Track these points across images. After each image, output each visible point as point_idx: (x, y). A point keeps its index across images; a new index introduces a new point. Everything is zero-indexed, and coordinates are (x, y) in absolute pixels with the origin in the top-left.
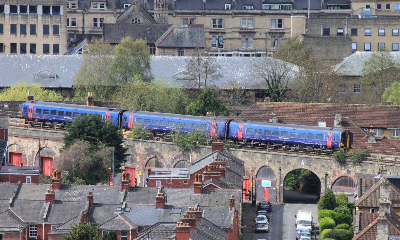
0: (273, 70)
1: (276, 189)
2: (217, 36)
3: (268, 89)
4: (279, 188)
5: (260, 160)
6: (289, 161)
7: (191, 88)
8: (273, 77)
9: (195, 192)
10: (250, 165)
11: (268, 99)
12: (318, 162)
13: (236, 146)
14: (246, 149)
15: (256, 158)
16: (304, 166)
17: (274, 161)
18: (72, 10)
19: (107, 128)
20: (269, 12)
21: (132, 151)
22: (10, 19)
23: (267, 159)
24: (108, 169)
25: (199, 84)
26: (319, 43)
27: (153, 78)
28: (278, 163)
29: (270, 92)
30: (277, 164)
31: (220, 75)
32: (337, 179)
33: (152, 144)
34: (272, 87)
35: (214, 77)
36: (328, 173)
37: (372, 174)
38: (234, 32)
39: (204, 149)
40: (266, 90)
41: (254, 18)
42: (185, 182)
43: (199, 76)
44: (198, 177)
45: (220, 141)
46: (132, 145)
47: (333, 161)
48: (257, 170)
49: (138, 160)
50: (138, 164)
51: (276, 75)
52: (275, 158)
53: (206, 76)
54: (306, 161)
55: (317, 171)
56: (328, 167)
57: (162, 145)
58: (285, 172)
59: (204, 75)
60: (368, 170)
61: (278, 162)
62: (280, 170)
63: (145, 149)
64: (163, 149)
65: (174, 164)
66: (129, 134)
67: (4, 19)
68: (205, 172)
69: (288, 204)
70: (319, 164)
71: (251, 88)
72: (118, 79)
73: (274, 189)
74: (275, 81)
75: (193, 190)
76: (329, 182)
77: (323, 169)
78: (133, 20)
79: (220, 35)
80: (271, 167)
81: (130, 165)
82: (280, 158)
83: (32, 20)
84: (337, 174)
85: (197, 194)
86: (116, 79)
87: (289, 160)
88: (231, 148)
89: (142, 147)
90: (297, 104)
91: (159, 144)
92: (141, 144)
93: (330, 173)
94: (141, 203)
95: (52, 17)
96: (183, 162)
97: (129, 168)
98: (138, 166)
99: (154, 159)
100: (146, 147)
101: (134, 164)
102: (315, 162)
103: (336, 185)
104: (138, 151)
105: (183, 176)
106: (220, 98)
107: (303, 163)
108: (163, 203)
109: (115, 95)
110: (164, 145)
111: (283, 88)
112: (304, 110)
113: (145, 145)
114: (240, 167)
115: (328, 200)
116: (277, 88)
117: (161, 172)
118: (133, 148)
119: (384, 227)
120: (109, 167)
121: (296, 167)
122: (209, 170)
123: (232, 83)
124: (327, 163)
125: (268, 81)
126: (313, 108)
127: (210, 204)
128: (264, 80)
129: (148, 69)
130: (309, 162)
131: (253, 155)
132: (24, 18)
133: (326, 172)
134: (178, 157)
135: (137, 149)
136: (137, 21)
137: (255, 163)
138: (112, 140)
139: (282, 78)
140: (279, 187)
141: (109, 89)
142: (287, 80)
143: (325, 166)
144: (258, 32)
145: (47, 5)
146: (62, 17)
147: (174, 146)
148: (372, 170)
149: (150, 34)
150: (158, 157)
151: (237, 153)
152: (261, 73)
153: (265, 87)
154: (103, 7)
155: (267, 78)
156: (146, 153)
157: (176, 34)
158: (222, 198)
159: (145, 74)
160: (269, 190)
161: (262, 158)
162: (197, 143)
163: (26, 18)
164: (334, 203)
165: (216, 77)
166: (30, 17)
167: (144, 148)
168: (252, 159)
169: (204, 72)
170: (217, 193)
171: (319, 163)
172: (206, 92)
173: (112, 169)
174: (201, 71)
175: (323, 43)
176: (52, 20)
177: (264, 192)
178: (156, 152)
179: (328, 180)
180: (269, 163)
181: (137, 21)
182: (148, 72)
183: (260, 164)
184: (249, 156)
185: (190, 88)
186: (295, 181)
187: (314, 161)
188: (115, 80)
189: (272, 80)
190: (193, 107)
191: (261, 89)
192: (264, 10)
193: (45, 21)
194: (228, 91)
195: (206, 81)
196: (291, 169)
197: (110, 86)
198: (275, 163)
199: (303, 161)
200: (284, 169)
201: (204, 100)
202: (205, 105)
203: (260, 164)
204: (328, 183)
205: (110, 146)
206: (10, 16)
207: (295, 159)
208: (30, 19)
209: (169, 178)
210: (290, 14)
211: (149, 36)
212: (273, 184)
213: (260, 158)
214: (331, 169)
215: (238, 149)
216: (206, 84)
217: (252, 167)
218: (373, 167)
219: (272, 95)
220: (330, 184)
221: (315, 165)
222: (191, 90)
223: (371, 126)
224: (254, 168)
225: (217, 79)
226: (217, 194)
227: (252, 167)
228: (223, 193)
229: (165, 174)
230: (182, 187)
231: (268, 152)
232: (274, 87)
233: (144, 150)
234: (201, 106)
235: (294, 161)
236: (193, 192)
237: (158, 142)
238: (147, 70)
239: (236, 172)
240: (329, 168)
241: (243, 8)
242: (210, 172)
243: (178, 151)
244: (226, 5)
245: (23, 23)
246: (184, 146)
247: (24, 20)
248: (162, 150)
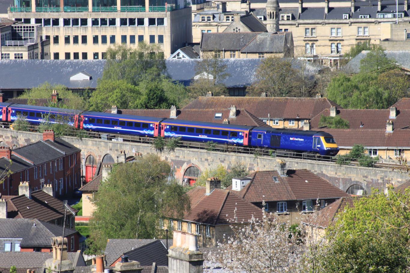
2: (336, 43)
17: (114, 150)
18: (208, 23)
20: (382, 20)
22: (121, 31)
26: (393, 46)
28: (116, 151)
30: (116, 152)
37: (183, 160)
38: (350, 39)
41: (368, 26)
60: (180, 156)
63: (25, 140)
67: (116, 31)
78: (234, 30)
79: (338, 42)
80: (112, 155)
82: (118, 145)
83: (140, 32)
95: (157, 28)
100: (26, 138)
119: (2, 209)
132: (133, 29)
136: (238, 30)
144: (373, 39)
145: (152, 18)
146: (166, 28)
148: (183, 156)
149: (242, 41)
154: (210, 20)
157: (259, 41)
163: (135, 30)
166: (138, 28)
175: (397, 46)
176: (157, 31)
181: (238, 30)
184: (96, 144)
192: (378, 18)
193: (151, 31)
198: (114, 152)
206: (121, 28)
208: (138, 31)
210: (380, 22)
211: (242, 44)
218: (183, 153)
223: (297, 118)
233: (24, 141)
241: (360, 17)
244: (344, 15)
245: (132, 34)
247: (133, 32)
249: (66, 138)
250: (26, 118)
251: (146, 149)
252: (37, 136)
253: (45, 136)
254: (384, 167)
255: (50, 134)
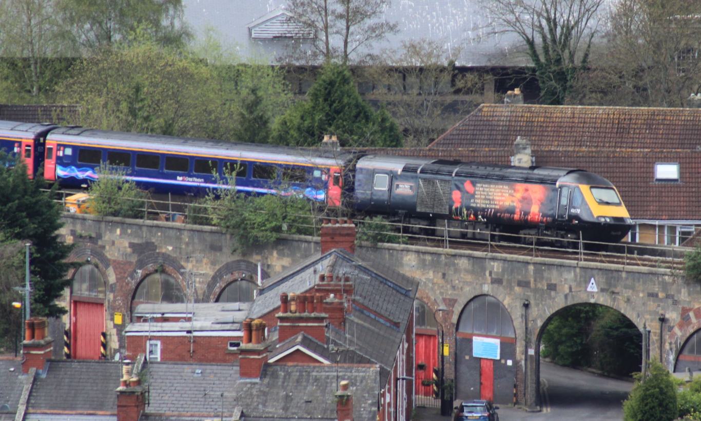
0: (547, 11)
1: (516, 363)
3: (532, 65)
4: (523, 362)
5: (469, 278)
6: (553, 282)
7: (302, 63)
8: (546, 29)
9: (243, 374)
10: (438, 292)
11: (515, 95)
12: (637, 285)
13: (399, 237)
14: (426, 245)
15: (457, 270)
16: (596, 296)
17: (509, 282)
19: (11, 185)
21: (94, 253)
23: (487, 273)
24: (14, 307)
25: (325, 51)
27: (188, 35)
29: (537, 73)
30: (517, 289)
31: (387, 24)
32: (692, 335)
33: (151, 232)
34: (542, 59)
35: (369, 33)
36: (667, 316)
39: (304, 245)
40: (528, 68)
42: (232, 345)
43: (326, 27)
44: (254, 328)
45: (345, 222)
46: (93, 235)
47: (680, 281)
48: (460, 309)
49: (112, 278)
50: (112, 291)
51: (555, 25)
52: (512, 271)
53: (348, 28)
54: (602, 280)
55: (633, 309)
56: (668, 297)
57: (181, 234)
58: (541, 313)
59: (342, 24)
61: (520, 284)
62: (526, 306)
63: (132, 245)
64: (183, 246)
65: (217, 290)
66: (84, 202)
68: (280, 314)
69: (549, 409)
70: (641, 288)
71: (483, 64)
72: (83, 36)
73: (510, 363)
74: (554, 41)
75: (238, 368)
76: (670, 344)
77: (652, 305)
80: (500, 298)
81: (87, 293)
82: (527, 270)
84: (694, 320)
85: (248, 380)
86: (80, 37)
87: (554, 276)
88: (383, 242)
89: (122, 240)
90: (601, 111)
91: (172, 233)
92: (118, 231)
93: (673, 316)
94: (81, 408)
96: (244, 283)
97: (84, 303)
98: (111, 296)
99: (157, 276)
100: (136, 241)
101: (100, 292)
102: (629, 282)
103: (692, 351)
104: (111, 254)
105: (228, 327)
106: (380, 94)
107: (593, 287)
108: (137, 406)
109: (67, 87)
110: (186, 233)
111: (576, 62)
112: (621, 129)
113: (130, 235)
114: (402, 298)
115: (652, 395)
116: (558, 61)
117: (166, 315)
118: (96, 244)
120: (15, 300)
121: (573, 297)
122: (293, 308)
123: (414, 49)
124: (664, 286)
125: (531, 43)
126: (650, 123)
127: (285, 409)
128: (521, 39)
129: (175, 7)
130: (610, 285)
131: (446, 264)
133: (661, 312)
134: (228, 268)
135: (107, 247)
137: (453, 287)
138: (27, 220)
139: (573, 32)
140: (523, 357)
141: (58, 68)
142: (587, 39)
143: (657, 295)
147: (216, 237)
150: (169, 269)
151: (402, 258)
152: (511, 17)
153: (524, 61)
155: (529, 32)
156: (134, 259)
158: (323, 392)
159: (165, 22)
160: (495, 369)
161: (472, 272)
162: (285, 227)
164: (671, 405)
165: (376, 32)
167: (127, 245)
168: (444, 275)
169: (341, 16)
170: (309, 375)
171: (639, 286)
172: (330, 74)
173: (24, 305)
174: (333, 12)
177: (481, 375)
178: (163, 254)
179: (667, 337)
180: (496, 286)
182: (173, 18)
183: (467, 289)
184: (435, 265)
185: (297, 64)
186: (579, 341)
187: (627, 279)
188: (74, 41)
189: (544, 38)
190: (291, 121)
191: (512, 65)
194: (404, 73)
195: (346, 43)
196: (559, 303)
197: (60, 60)
198: (511, 289)
199: (592, 281)
200: (537, 305)
201: (326, 100)
202: (327, 115)
203: (467, 289)
204: (667, 346)
205: (19, 236)
207: (570, 276)
209: (184, 334)
212: (507, 348)
213: (467, 271)
214: (676, 303)
215: (403, 246)
216: (345, 52)
217: (444, 300)
219: (543, 82)
220: (674, 349)
221: (628, 293)
222: (301, 69)
224: (450, 300)
225: (379, 36)
226: (308, 381)
227: (444, 300)
228: (328, 377)
229: (176, 320)
230: (225, 361)
231: (490, 254)
232: (548, 60)
233: (129, 250)
234: (317, 118)
235: (566, 280)
236: (238, 375)
237: (170, 224)
238: (171, 12)
239: (386, 314)
240: (670, 301)
242: (297, 314)
243: (227, 250)
246: (247, 237)
248: (180, 248)
249: (309, 242)
250: (123, 175)
251: (644, 283)
252: (144, 229)
253: (328, 238)
254: (184, 318)
255: (346, 232)
